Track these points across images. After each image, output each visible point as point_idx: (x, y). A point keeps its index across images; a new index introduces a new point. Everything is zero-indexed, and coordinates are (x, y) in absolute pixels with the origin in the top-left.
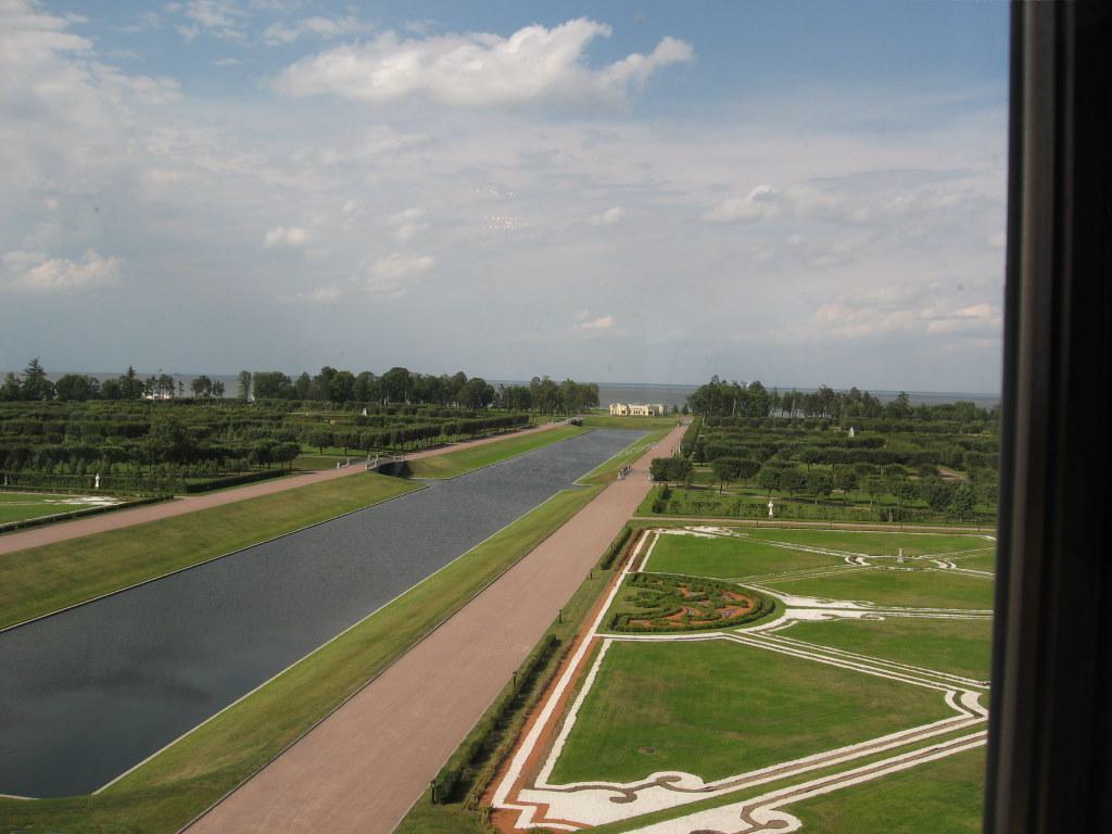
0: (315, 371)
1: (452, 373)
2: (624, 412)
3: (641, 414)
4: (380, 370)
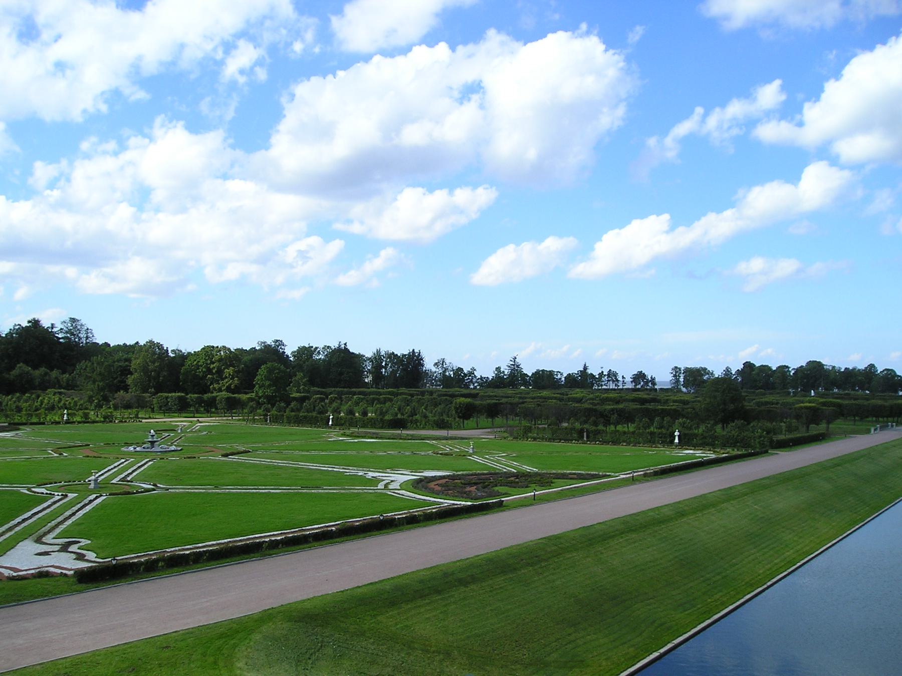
0: (736, 366)
4: (795, 361)
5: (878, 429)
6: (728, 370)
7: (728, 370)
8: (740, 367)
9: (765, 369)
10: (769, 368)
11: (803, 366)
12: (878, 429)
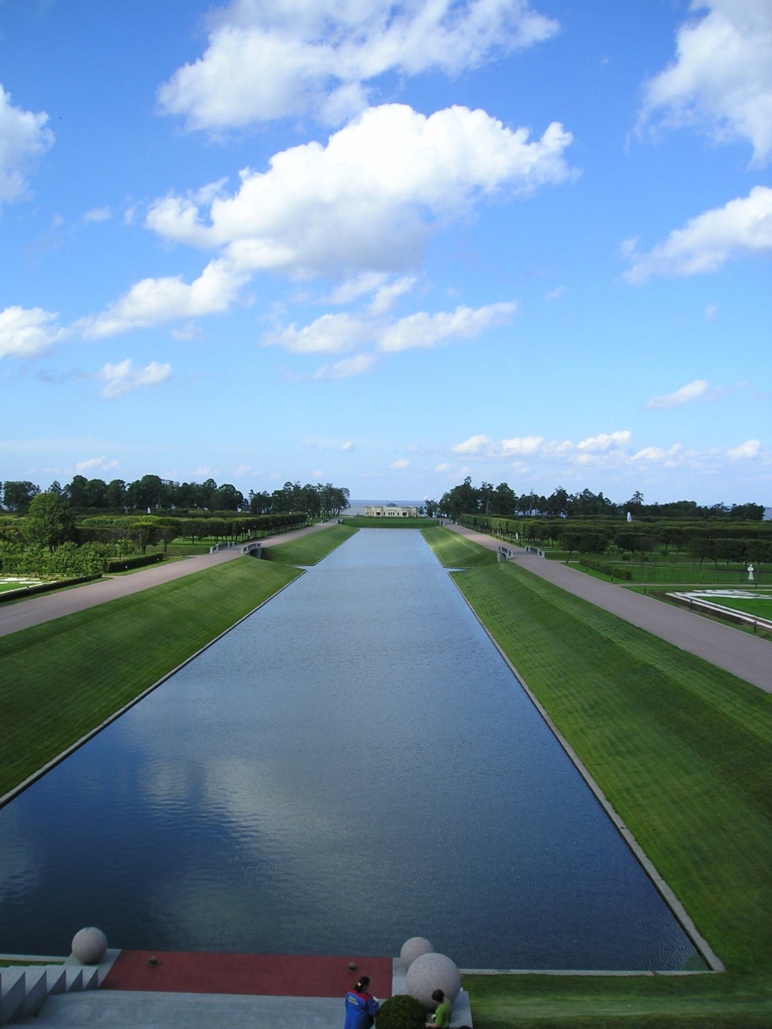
1: (200, 482)
2: (378, 514)
3: (396, 515)
4: (131, 476)
5: (217, 549)
6: (56, 486)
7: (56, 486)
8: (70, 481)
9: (97, 483)
10: (103, 483)
11: (139, 481)
12: (217, 549)
